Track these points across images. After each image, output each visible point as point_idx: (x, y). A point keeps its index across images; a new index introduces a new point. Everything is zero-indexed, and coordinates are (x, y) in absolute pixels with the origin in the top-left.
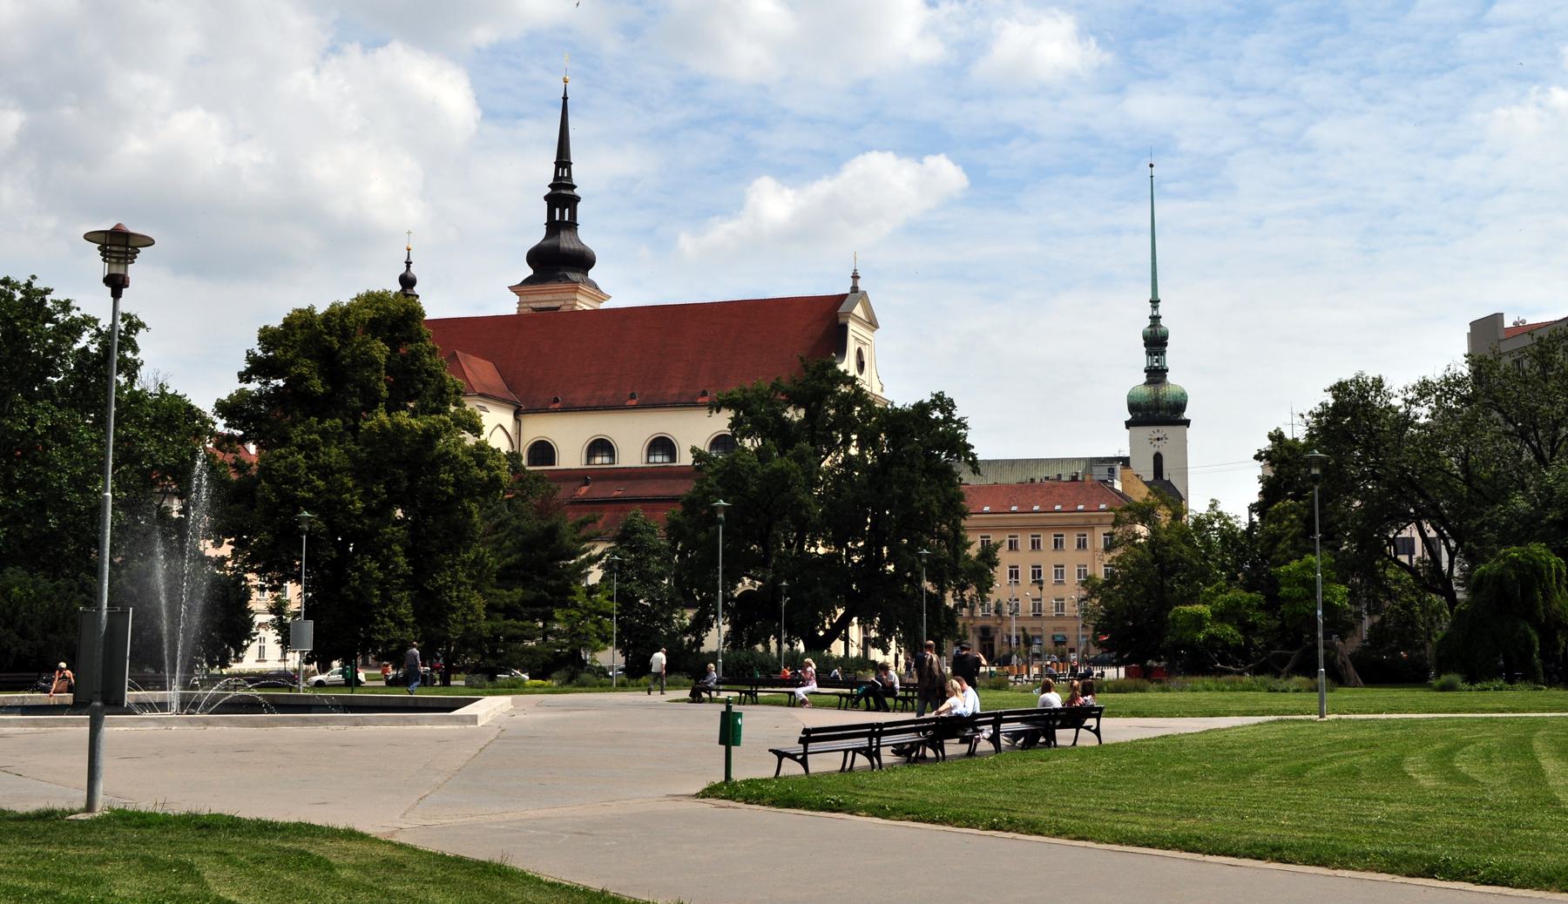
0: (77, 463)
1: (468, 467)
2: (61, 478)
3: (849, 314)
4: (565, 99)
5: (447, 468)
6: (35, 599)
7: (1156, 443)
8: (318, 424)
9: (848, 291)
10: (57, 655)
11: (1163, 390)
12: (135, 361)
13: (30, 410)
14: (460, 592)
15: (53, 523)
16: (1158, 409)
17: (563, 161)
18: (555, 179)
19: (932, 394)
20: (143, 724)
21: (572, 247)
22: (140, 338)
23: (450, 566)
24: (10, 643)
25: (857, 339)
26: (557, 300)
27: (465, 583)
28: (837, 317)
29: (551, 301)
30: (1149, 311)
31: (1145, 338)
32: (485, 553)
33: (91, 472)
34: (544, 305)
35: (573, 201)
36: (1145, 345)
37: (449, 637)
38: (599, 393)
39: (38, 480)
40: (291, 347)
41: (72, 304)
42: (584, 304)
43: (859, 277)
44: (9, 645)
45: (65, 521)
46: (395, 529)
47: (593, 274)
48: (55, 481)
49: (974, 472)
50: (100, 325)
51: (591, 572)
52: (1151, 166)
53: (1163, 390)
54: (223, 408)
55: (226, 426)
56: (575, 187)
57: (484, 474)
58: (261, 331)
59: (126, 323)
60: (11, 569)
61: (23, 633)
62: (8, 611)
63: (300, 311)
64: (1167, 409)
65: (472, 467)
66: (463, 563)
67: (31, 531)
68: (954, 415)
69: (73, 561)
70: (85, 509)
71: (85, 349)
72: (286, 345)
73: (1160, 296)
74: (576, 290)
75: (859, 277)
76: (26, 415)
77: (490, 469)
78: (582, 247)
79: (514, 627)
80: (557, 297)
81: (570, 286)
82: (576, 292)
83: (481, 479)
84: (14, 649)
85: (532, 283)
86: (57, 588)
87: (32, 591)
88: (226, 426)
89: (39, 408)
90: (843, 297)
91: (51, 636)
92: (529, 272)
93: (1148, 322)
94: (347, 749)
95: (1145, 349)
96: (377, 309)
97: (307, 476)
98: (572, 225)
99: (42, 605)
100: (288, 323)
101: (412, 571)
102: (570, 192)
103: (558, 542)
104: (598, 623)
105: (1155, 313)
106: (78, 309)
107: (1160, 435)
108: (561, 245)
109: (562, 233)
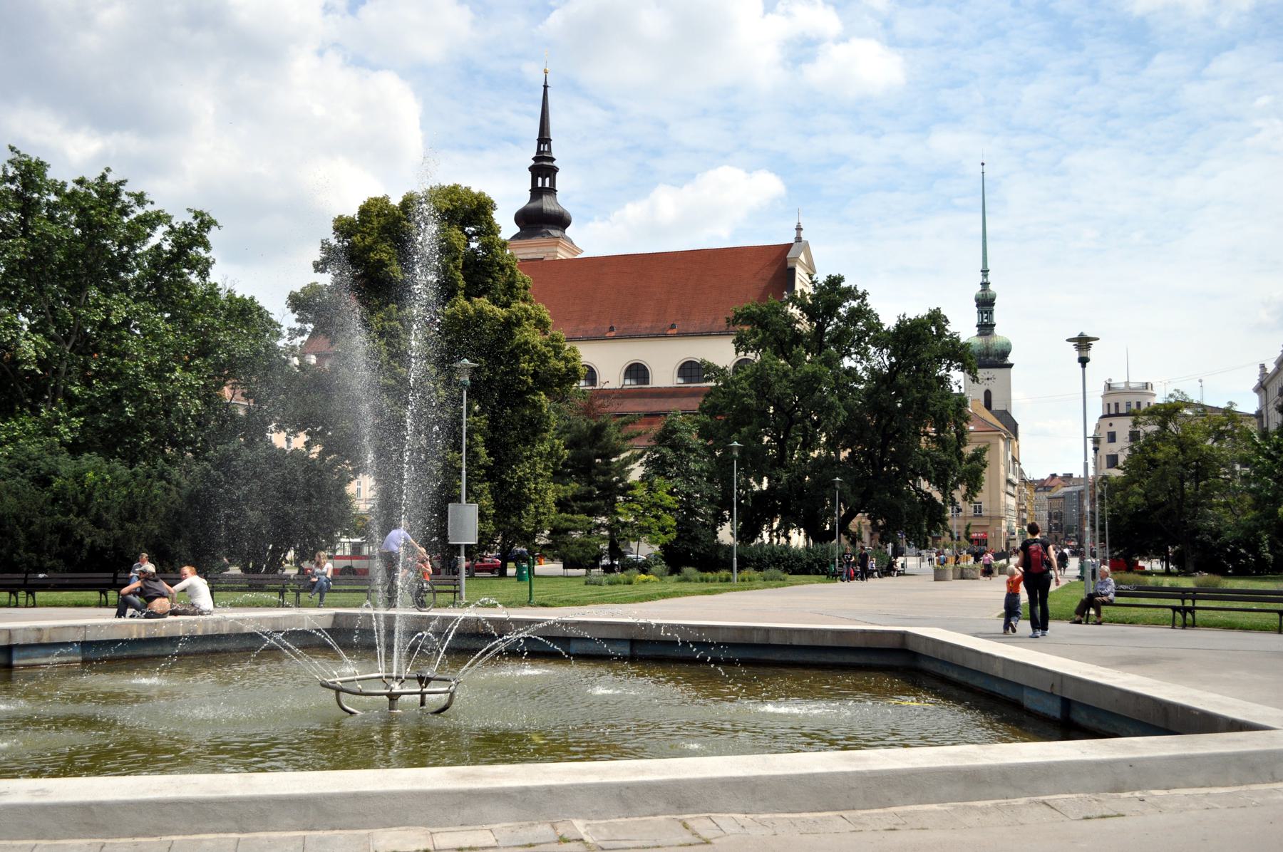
0: (153, 353)
1: (546, 356)
2: (137, 366)
3: (796, 259)
4: (546, 87)
5: (527, 357)
6: (111, 485)
7: (986, 382)
8: (397, 312)
9: (792, 241)
10: (136, 547)
11: (992, 340)
12: (207, 260)
13: (106, 301)
14: (537, 484)
15: (130, 411)
16: (988, 355)
17: (544, 138)
18: (537, 153)
19: (930, 310)
20: (467, 812)
21: (553, 208)
22: (212, 236)
23: (528, 458)
24: (83, 533)
25: (801, 281)
26: (541, 253)
27: (541, 475)
28: (786, 261)
29: (536, 253)
30: (980, 278)
31: (977, 300)
32: (560, 445)
33: (167, 361)
34: (530, 257)
35: (552, 172)
36: (977, 306)
37: (523, 529)
38: (581, 327)
39: (114, 370)
40: (369, 234)
41: (147, 197)
42: (562, 255)
43: (801, 229)
44: (81, 536)
45: (142, 410)
46: (476, 419)
47: (569, 231)
48: (131, 369)
49: (973, 381)
50: (173, 223)
51: (632, 469)
52: (983, 164)
53: (992, 340)
54: (298, 303)
55: (297, 320)
56: (554, 160)
57: (561, 365)
58: (336, 221)
59: (198, 220)
60: (87, 455)
61: (98, 522)
62: (81, 498)
63: (376, 199)
64: (995, 356)
65: (550, 358)
66: (540, 454)
67: (108, 420)
68: (947, 330)
69: (149, 452)
70: (162, 397)
71: (158, 247)
72: (363, 232)
73: (989, 267)
74: (557, 244)
75: (801, 229)
76: (102, 306)
77: (567, 360)
78: (561, 210)
79: (566, 520)
80: (541, 249)
81: (553, 240)
82: (556, 246)
83: (559, 370)
84: (88, 540)
85: (519, 239)
86: (135, 475)
87: (108, 477)
88: (297, 320)
89: (115, 300)
90: (789, 246)
91: (128, 525)
92: (517, 230)
93: (980, 287)
94: (892, 827)
95: (977, 309)
96: (451, 200)
97: (389, 364)
98: (552, 191)
99: (119, 492)
100: (364, 211)
101: (493, 462)
102: (550, 164)
103: (605, 440)
104: (658, 518)
105: (985, 280)
106: (152, 203)
107: (990, 376)
108: (544, 208)
109: (544, 197)
